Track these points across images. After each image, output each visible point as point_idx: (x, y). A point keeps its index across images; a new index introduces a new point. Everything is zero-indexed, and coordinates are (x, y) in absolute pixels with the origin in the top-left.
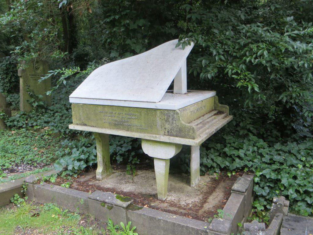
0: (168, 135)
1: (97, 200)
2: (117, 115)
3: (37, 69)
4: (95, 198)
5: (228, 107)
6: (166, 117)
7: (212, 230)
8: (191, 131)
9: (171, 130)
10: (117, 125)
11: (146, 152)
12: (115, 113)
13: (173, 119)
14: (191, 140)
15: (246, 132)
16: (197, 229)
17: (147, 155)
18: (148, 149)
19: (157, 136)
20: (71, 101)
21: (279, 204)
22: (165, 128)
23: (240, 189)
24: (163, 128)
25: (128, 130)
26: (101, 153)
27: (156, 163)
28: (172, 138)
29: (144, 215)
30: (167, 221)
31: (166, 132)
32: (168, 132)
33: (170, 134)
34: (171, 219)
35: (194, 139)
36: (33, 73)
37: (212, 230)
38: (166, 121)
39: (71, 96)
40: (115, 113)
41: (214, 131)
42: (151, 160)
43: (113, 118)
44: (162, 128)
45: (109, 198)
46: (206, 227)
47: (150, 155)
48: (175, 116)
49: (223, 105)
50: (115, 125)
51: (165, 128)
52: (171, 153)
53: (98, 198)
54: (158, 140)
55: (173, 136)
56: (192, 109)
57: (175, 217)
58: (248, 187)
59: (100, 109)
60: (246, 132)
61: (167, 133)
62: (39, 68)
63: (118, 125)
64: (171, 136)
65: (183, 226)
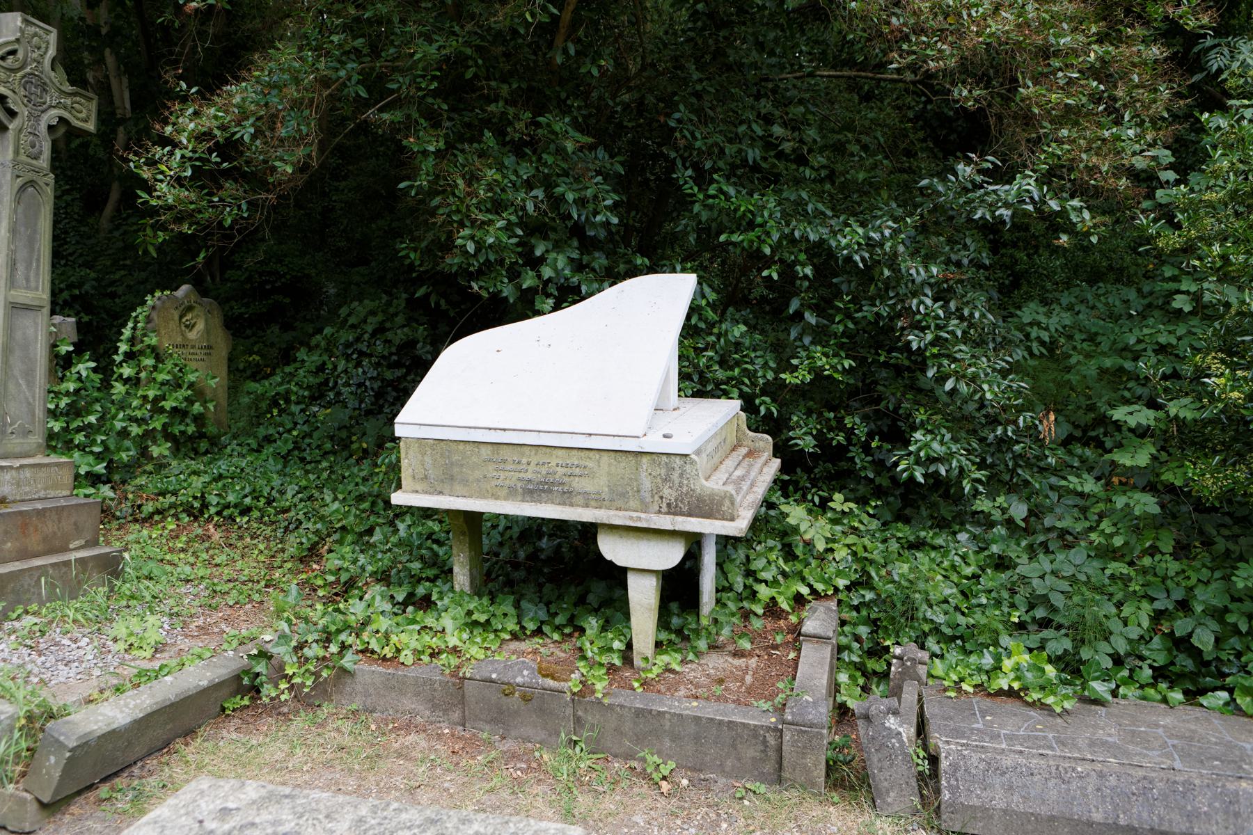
0: (668, 513)
1: (492, 681)
2: (531, 468)
3: (191, 327)
4: (485, 674)
5: (770, 439)
6: (663, 472)
7: (792, 724)
8: (727, 503)
10: (533, 492)
11: (608, 556)
12: (529, 464)
13: (681, 475)
15: (1176, 272)
16: (756, 726)
17: (611, 562)
18: (612, 549)
19: (643, 515)
20: (399, 431)
21: (909, 659)
22: (662, 498)
24: (656, 498)
25: (563, 504)
26: (466, 571)
27: (633, 581)
28: (679, 519)
29: (622, 706)
30: (681, 715)
31: (664, 505)
32: (669, 505)
33: (673, 510)
34: (687, 709)
35: (732, 519)
36: (179, 340)
37: (792, 724)
40: (529, 464)
42: (618, 575)
43: (522, 475)
44: (653, 497)
45: (526, 672)
46: (773, 720)
47: (620, 562)
48: (688, 467)
49: (760, 435)
50: (531, 492)
51: (662, 498)
52: (670, 556)
53: (494, 676)
54: (644, 525)
55: (682, 514)
56: (710, 448)
57: (695, 704)
59: (486, 452)
60: (1176, 272)
61: (665, 509)
62: (193, 326)
63: (531, 492)
64: (675, 514)
65: (721, 723)
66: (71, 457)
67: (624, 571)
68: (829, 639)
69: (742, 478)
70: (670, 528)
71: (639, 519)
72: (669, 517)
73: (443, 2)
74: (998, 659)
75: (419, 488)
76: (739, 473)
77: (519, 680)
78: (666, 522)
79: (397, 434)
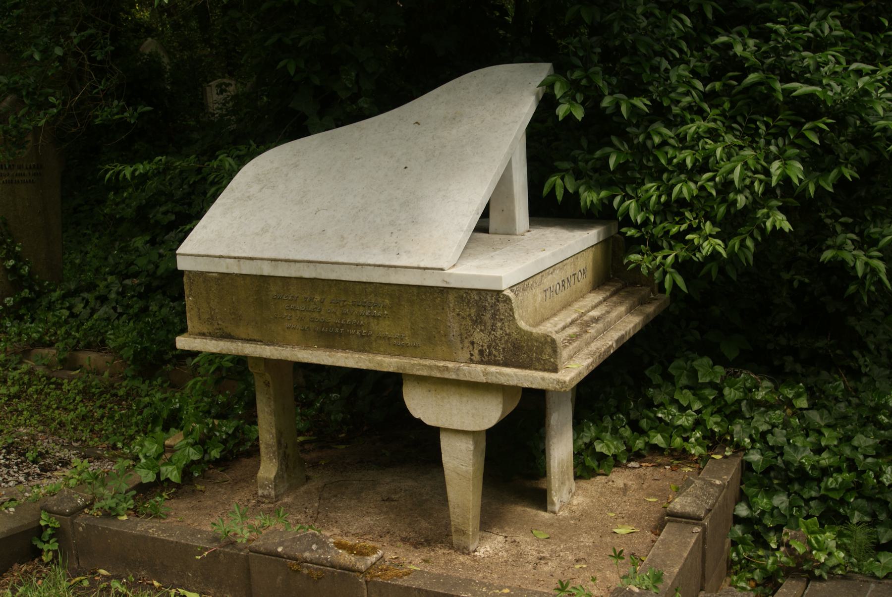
1: (278, 555)
6: (473, 311)
8: (549, 350)
9: (489, 347)
12: (322, 302)
13: (494, 316)
14: (546, 375)
19: (450, 365)
22: (473, 343)
23: (689, 509)
28: (493, 369)
31: (476, 352)
32: (481, 352)
33: (486, 358)
35: (555, 370)
38: (475, 322)
39: (183, 249)
41: (611, 346)
47: (430, 420)
48: (501, 306)
51: (473, 343)
53: (280, 549)
55: (496, 363)
58: (714, 505)
61: (476, 357)
64: (489, 363)
66: (775, 441)
67: (434, 433)
68: (699, 519)
69: (596, 320)
70: (483, 379)
71: (447, 369)
72: (480, 368)
73: (9, 311)
74: (27, 334)
75: (205, 331)
76: (595, 313)
77: (307, 554)
78: (478, 372)
79: (180, 268)
